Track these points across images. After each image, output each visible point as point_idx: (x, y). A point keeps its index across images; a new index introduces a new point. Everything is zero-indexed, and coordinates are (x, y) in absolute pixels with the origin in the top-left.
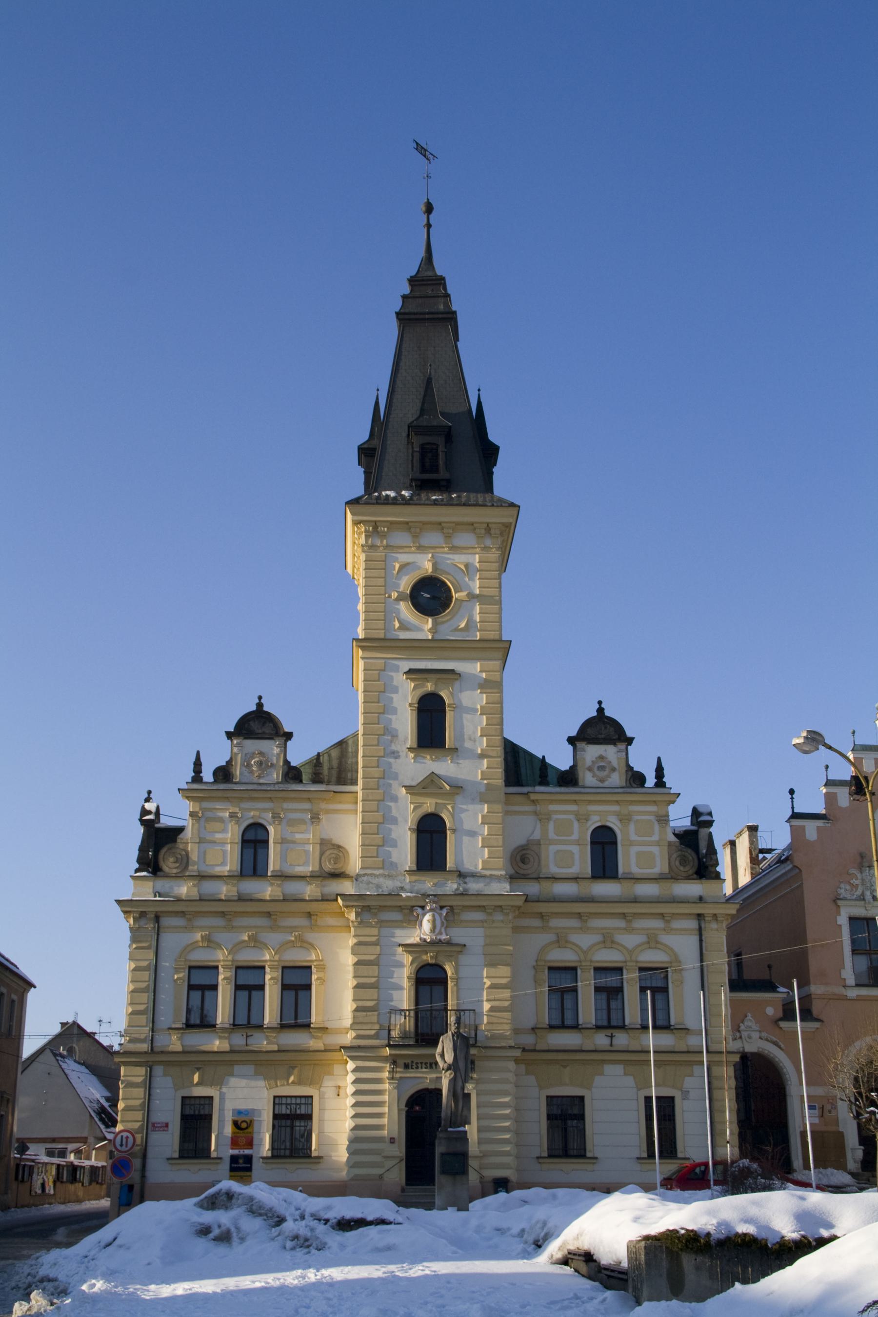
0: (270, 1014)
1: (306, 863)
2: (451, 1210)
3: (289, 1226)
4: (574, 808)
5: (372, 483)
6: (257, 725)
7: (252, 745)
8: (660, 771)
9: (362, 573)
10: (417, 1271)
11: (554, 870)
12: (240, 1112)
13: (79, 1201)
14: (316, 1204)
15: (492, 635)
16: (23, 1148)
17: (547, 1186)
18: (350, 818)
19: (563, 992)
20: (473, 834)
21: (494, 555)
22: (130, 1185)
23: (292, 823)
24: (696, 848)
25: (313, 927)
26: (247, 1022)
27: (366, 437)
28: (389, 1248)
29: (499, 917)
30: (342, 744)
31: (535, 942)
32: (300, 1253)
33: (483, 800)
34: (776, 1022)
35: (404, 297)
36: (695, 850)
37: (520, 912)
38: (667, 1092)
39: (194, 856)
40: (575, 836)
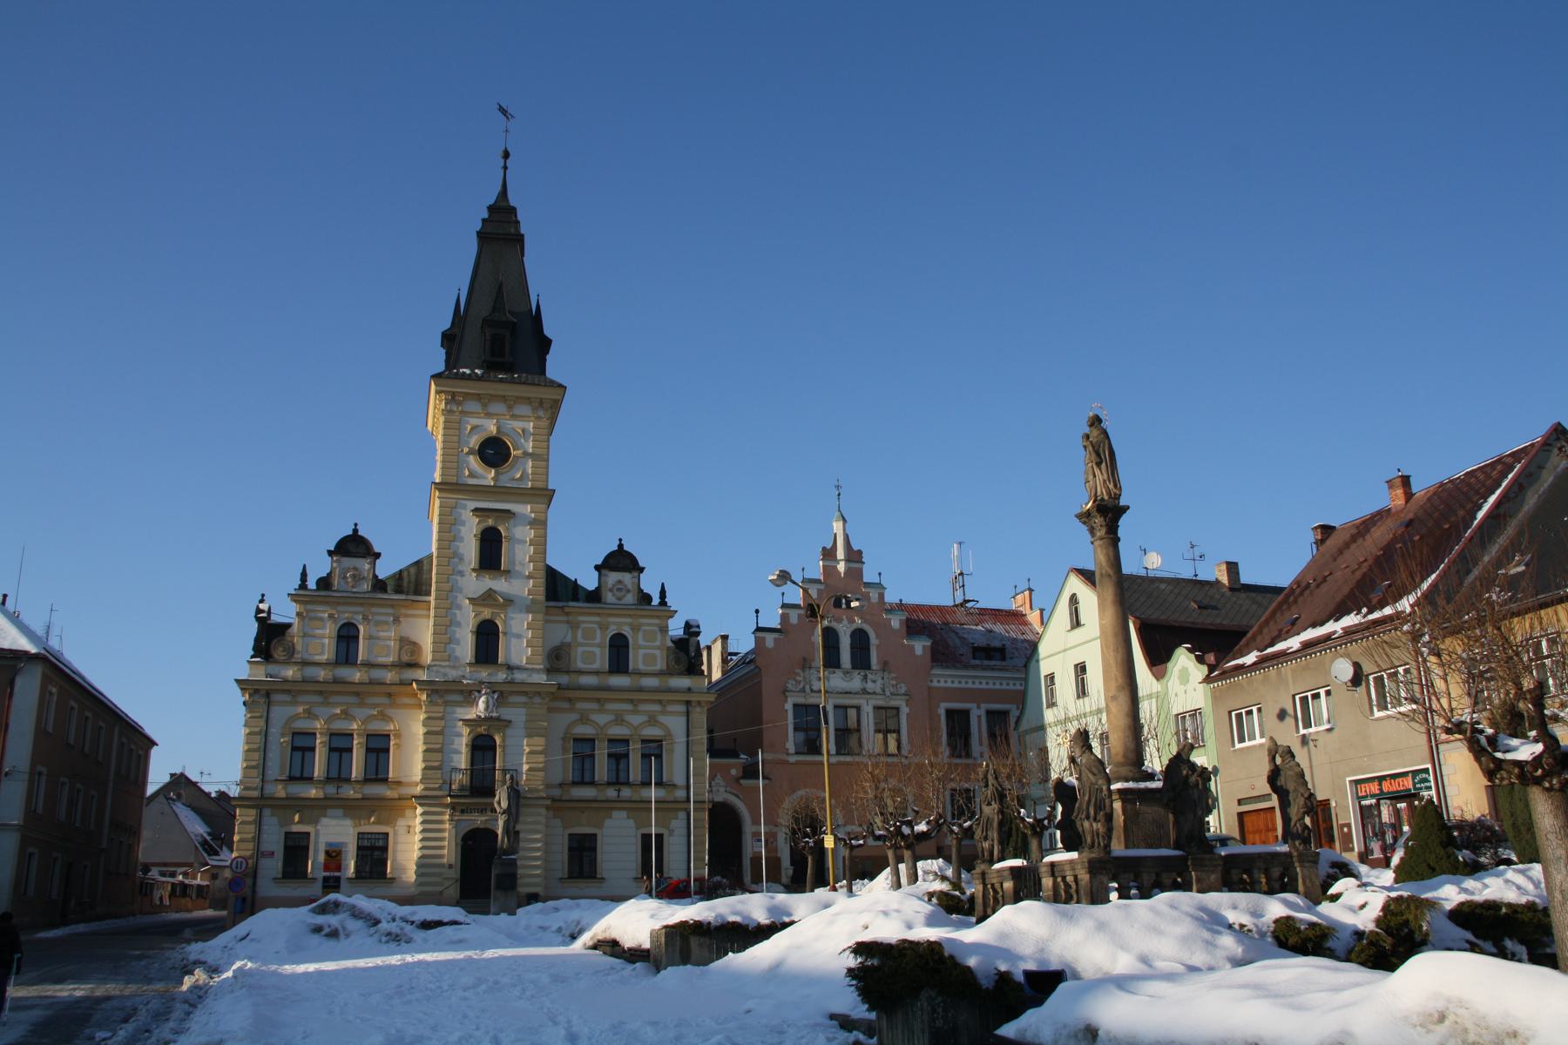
0: (357, 769)
1: (388, 655)
2: (503, 916)
3: (384, 926)
4: (597, 619)
5: (451, 362)
6: (353, 546)
7: (348, 562)
8: (663, 593)
9: (441, 431)
10: (490, 953)
11: (580, 665)
12: (329, 844)
13: (188, 911)
14: (406, 910)
15: (540, 484)
16: (146, 868)
17: (572, 898)
18: (424, 621)
19: (583, 758)
20: (519, 636)
21: (545, 423)
22: (242, 899)
23: (378, 623)
24: (687, 651)
25: (393, 705)
26: (338, 776)
27: (448, 325)
28: (461, 941)
29: (537, 700)
30: (418, 563)
31: (564, 720)
32: (393, 945)
33: (528, 611)
34: (737, 780)
35: (484, 220)
36: (687, 653)
37: (554, 697)
38: (661, 831)
39: (299, 647)
40: (598, 640)
